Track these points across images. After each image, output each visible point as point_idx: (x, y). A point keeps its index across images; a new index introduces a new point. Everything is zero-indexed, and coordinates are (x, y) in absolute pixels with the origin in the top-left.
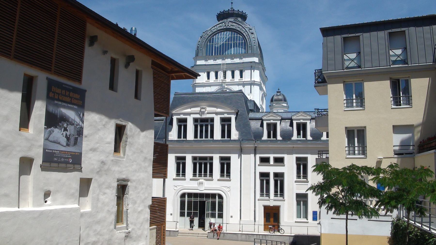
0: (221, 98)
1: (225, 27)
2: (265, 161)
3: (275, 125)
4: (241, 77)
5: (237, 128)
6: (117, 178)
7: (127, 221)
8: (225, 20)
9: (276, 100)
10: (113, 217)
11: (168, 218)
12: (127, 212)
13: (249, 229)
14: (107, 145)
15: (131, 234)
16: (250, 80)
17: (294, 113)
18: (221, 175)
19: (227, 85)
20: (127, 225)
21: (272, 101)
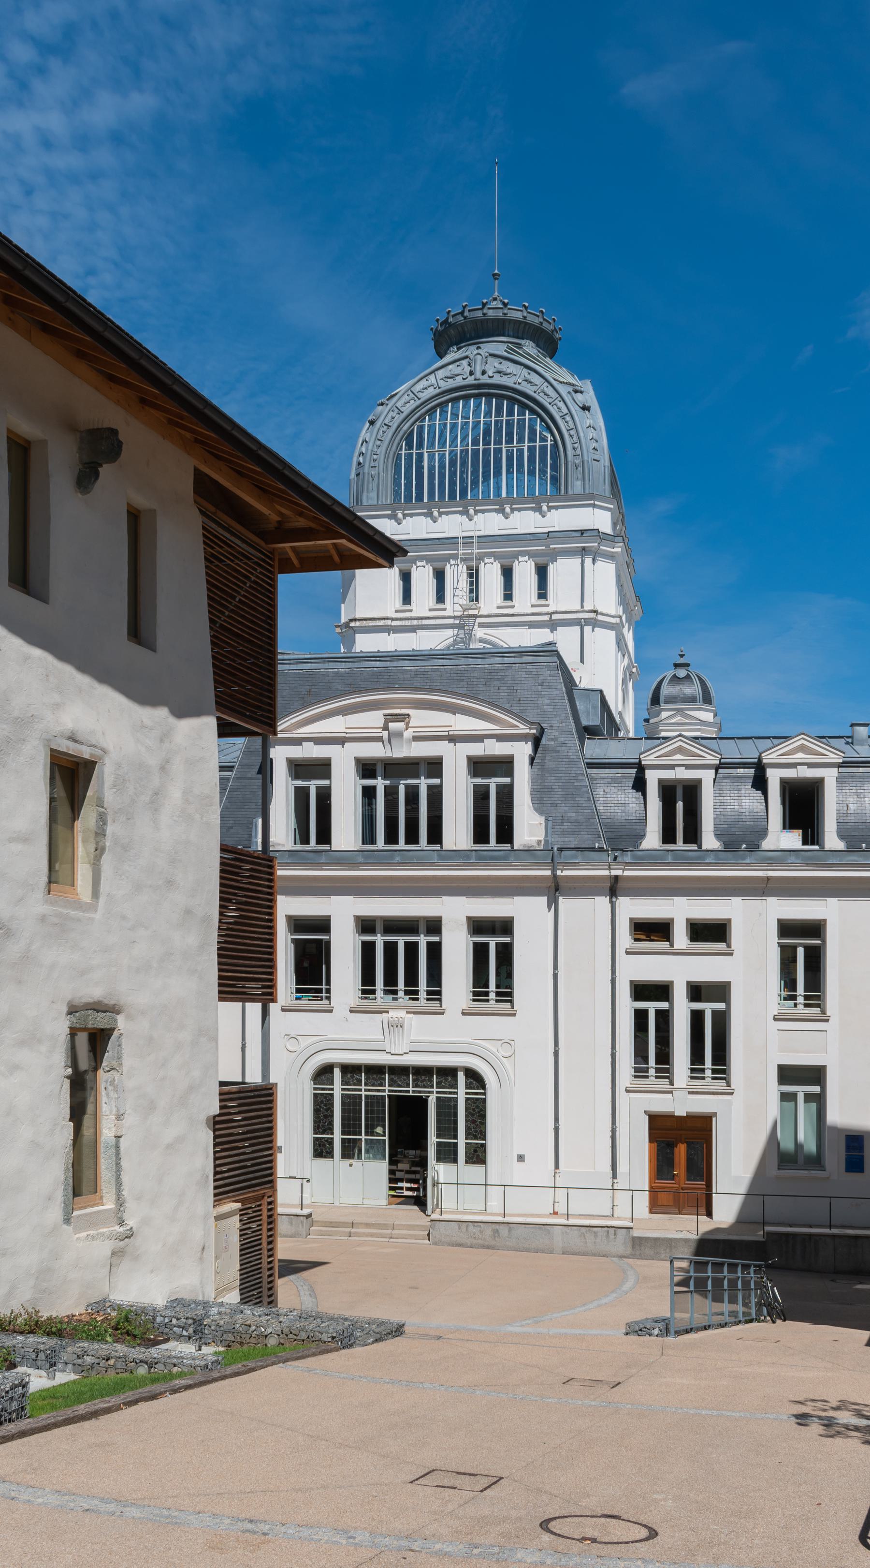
0: (461, 675)
1: (471, 380)
2: (653, 931)
3: (692, 791)
4: (542, 594)
5: (540, 802)
6: (69, 997)
7: (119, 1184)
8: (471, 351)
9: (671, 700)
10: (55, 1173)
11: (283, 1166)
12: (117, 1147)
13: (590, 1207)
14: (17, 847)
15: (136, 1241)
16: (579, 608)
17: (776, 741)
18: (475, 994)
19: (482, 625)
20: (120, 1202)
21: (655, 700)
